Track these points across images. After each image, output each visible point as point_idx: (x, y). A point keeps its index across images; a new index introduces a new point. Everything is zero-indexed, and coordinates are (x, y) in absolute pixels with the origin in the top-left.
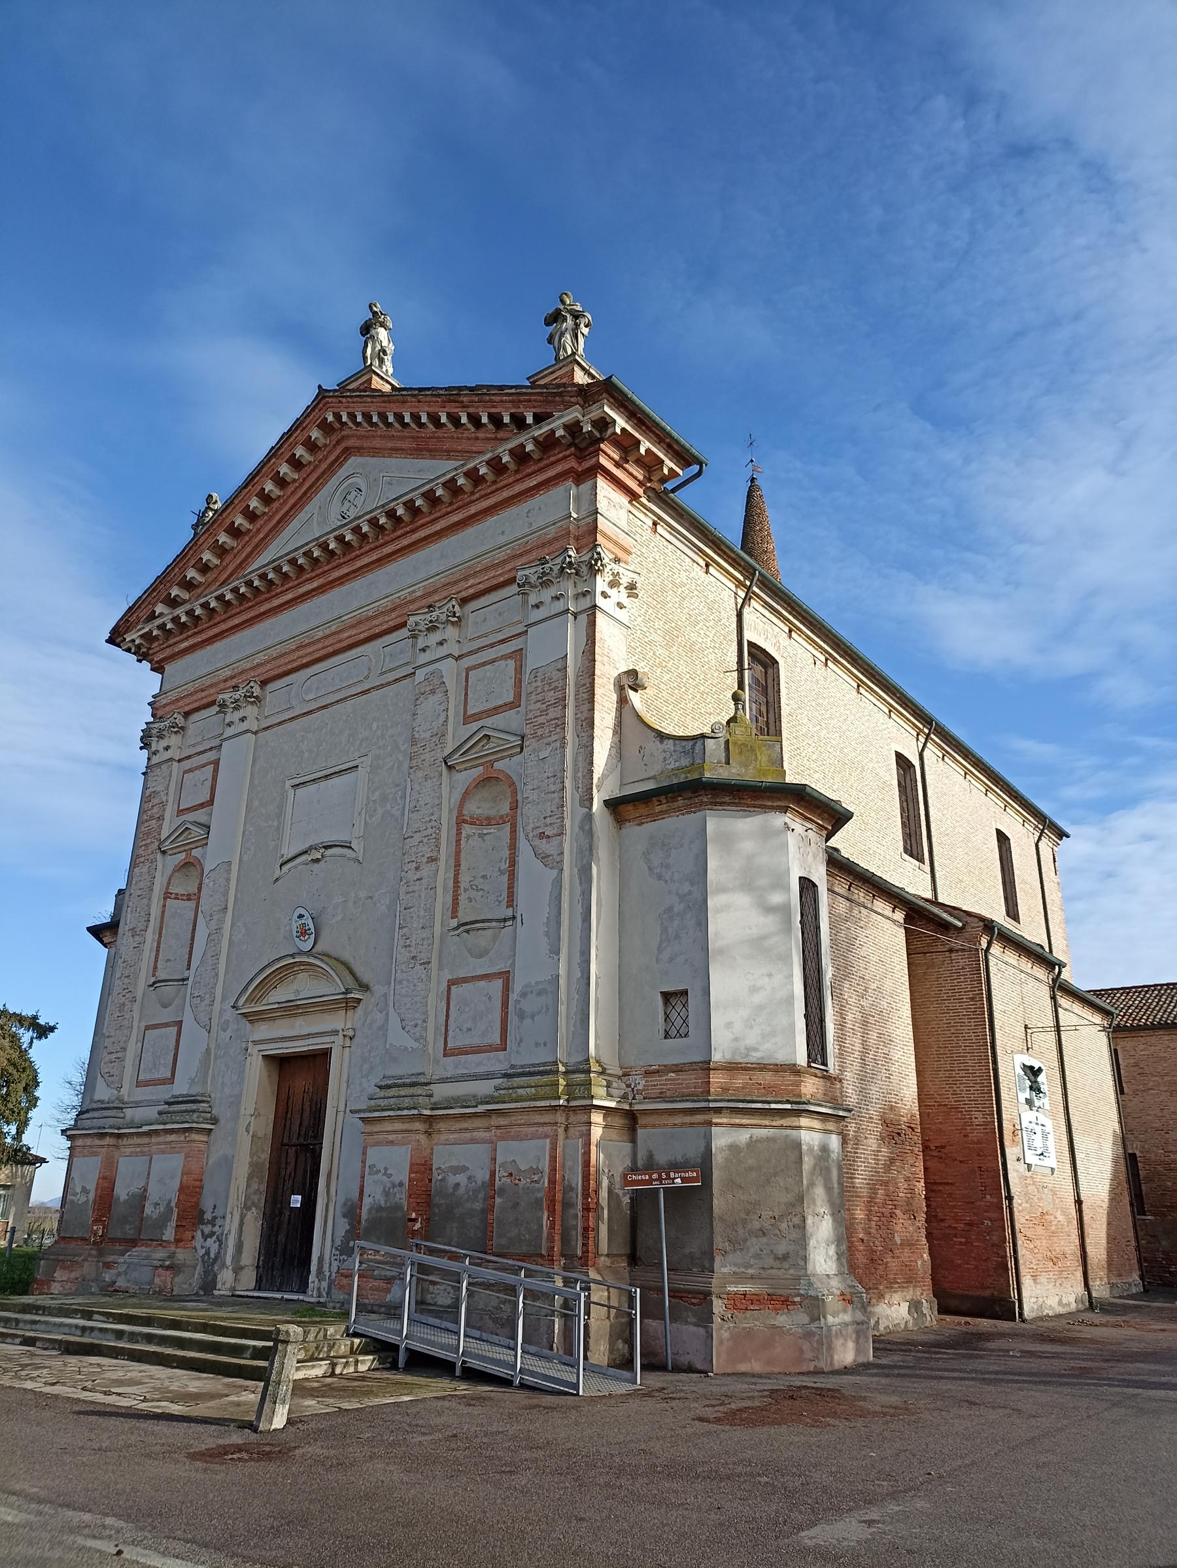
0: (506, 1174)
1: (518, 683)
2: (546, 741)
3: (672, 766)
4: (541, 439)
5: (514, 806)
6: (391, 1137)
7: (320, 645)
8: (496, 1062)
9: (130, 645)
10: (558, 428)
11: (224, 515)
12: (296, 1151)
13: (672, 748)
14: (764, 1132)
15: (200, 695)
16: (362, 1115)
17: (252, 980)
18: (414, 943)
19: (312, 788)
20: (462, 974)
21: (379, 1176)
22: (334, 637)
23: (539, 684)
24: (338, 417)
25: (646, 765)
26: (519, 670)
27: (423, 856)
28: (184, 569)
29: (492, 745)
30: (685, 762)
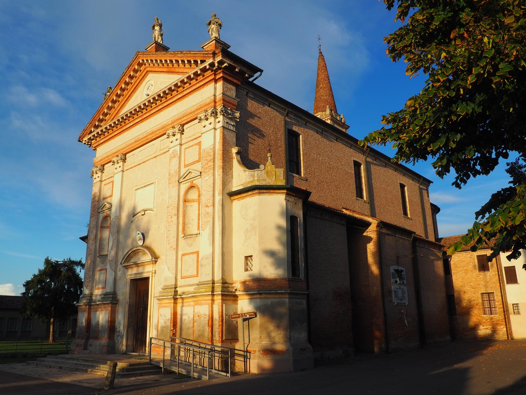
1: (200, 154)
2: (207, 174)
3: (248, 181)
6: (166, 305)
7: (142, 141)
8: (196, 281)
9: (85, 142)
11: (110, 96)
12: (143, 309)
14: (276, 300)
19: (141, 190)
22: (145, 138)
23: (205, 154)
24: (143, 60)
26: (200, 149)
28: (99, 116)
29: (192, 175)
30: (252, 179)
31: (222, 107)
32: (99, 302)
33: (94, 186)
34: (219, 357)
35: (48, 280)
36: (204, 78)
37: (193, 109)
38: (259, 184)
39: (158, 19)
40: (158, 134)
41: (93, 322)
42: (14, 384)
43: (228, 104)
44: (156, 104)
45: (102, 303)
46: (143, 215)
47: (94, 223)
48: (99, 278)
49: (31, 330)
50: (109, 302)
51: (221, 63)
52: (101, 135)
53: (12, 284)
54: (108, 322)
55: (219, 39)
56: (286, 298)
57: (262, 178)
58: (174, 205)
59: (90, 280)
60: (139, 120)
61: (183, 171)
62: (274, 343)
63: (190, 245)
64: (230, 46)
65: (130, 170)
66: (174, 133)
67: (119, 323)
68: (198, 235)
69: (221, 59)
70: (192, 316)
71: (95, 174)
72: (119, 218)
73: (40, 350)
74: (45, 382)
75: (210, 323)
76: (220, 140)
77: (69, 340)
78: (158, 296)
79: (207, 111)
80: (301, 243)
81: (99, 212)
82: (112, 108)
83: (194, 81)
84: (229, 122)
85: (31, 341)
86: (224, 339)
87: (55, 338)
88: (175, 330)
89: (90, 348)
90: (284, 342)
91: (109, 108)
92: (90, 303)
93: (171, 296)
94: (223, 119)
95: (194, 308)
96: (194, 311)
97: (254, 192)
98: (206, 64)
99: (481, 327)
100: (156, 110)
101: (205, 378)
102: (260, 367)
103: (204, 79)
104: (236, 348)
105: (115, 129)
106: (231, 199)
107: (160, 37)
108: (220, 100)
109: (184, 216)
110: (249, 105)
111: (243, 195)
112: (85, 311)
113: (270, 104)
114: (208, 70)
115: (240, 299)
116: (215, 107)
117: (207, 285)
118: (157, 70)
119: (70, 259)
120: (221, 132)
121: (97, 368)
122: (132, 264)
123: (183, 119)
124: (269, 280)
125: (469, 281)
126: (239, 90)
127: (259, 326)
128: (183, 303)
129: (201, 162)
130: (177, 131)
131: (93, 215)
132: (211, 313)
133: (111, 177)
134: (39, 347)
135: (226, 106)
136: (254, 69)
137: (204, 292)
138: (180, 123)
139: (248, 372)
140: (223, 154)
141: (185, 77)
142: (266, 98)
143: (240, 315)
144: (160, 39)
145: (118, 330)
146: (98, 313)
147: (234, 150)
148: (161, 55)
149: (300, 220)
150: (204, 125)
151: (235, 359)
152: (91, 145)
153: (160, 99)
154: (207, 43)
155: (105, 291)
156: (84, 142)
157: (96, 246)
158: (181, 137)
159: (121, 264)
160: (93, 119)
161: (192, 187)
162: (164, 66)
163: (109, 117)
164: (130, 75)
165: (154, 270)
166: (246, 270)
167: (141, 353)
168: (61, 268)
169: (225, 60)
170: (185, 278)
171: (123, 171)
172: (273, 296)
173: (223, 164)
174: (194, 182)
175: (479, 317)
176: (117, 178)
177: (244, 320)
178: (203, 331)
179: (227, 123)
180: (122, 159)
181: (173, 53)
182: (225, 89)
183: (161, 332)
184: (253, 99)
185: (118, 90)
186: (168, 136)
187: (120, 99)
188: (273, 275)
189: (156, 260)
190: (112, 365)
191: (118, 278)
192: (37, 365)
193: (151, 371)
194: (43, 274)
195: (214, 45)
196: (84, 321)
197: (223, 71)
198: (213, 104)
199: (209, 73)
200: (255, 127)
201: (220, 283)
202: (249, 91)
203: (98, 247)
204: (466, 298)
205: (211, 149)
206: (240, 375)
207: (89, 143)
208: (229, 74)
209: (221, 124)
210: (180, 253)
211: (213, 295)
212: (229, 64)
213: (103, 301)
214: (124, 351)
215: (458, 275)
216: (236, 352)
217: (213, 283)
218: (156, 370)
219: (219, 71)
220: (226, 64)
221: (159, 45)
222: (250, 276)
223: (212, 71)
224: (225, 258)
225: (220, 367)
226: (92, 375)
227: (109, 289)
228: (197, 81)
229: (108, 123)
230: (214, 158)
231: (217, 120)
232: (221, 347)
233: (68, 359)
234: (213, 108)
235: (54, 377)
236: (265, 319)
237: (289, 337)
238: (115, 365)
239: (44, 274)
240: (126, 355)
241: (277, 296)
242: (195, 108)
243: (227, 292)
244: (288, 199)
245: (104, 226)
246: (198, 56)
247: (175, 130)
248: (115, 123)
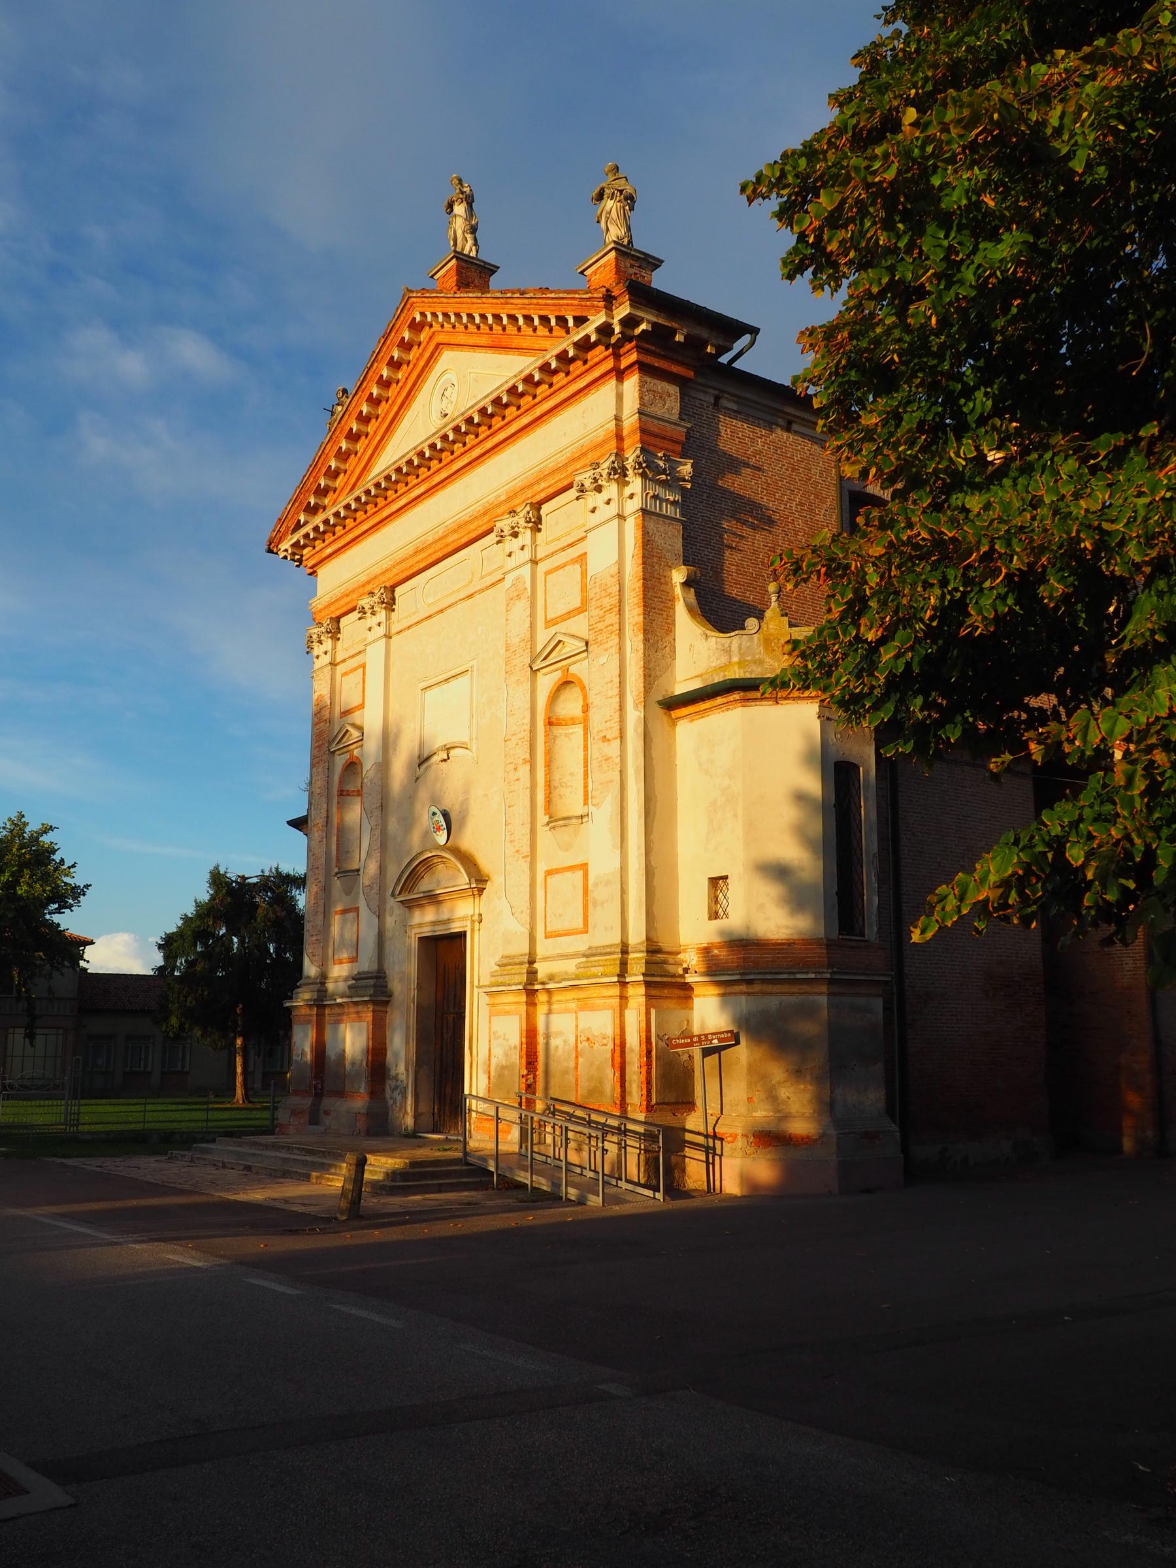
1: (584, 588)
2: (605, 646)
3: (713, 665)
4: (581, 343)
5: (586, 708)
6: (507, 1008)
8: (580, 944)
9: (285, 553)
11: (343, 422)
14: (793, 999)
16: (488, 990)
17: (403, 872)
19: (437, 689)
23: (598, 590)
24: (423, 314)
26: (584, 574)
28: (316, 478)
29: (567, 649)
30: (724, 660)
31: (638, 452)
32: (342, 997)
33: (316, 678)
34: (640, 1149)
35: (223, 931)
36: (587, 366)
37: (562, 459)
38: (743, 676)
39: (460, 181)
41: (331, 1053)
42: (134, 1203)
43: (657, 442)
44: (464, 444)
45: (349, 1000)
46: (445, 760)
47: (319, 783)
48: (342, 936)
49: (186, 1069)
50: (366, 999)
51: (629, 322)
52: (324, 532)
53: (132, 936)
54: (368, 1052)
55: (630, 242)
57: (753, 655)
58: (522, 735)
59: (319, 937)
61: (543, 636)
62: (786, 1117)
63: (566, 847)
64: (663, 261)
66: (516, 529)
67: (396, 1055)
68: (584, 820)
69: (628, 311)
70: (572, 1040)
71: (315, 645)
72: (384, 766)
73: (204, 1124)
74: (204, 1199)
75: (618, 1060)
76: (635, 548)
77: (277, 1099)
78: (488, 983)
79: (598, 466)
80: (869, 841)
81: (334, 752)
82: (350, 455)
83: (560, 379)
84: (662, 495)
85: (189, 1100)
86: (654, 1101)
87: (250, 1093)
88: (531, 1076)
89: (327, 1120)
91: (343, 456)
92: (321, 1001)
93: (520, 984)
94: (644, 489)
95: (577, 1018)
96: (577, 1026)
98: (590, 329)
101: (595, 1201)
102: (746, 1179)
103: (587, 371)
104: (688, 1127)
105: (360, 515)
106: (670, 716)
107: (469, 236)
108: (633, 432)
109: (548, 764)
110: (726, 432)
111: (703, 706)
112: (309, 1022)
113: (790, 423)
114: (595, 344)
115: (698, 996)
116: (619, 454)
117: (608, 957)
119: (277, 869)
120: (637, 525)
121: (333, 1171)
122: (422, 895)
123: (537, 488)
124: (773, 944)
126: (693, 393)
128: (549, 1003)
129: (586, 613)
130: (522, 522)
131: (317, 760)
132: (618, 1031)
133: (360, 652)
134: (202, 1115)
135: (652, 449)
136: (732, 329)
137: (600, 977)
138: (528, 499)
139: (718, 1191)
140: (646, 588)
141: (535, 369)
142: (775, 405)
143: (695, 1039)
144: (470, 242)
145: (393, 1073)
146: (342, 1026)
147: (678, 576)
148: (467, 300)
149: (867, 773)
150: (591, 507)
151: (685, 1156)
152: (300, 561)
153: (472, 429)
154: (594, 260)
155: (356, 969)
156: (282, 555)
157: (328, 845)
158: (534, 540)
159: (393, 895)
160: (302, 490)
161: (566, 683)
162: (482, 331)
163: (345, 480)
164: (392, 357)
165: (477, 912)
166: (714, 915)
167: (454, 1134)
168: (255, 898)
169: (640, 314)
170: (556, 936)
171: (388, 636)
172: (785, 988)
173: (644, 618)
174: (572, 669)
176: (375, 656)
177: (707, 1053)
178: (601, 1081)
179: (655, 497)
180: (383, 602)
181: (499, 295)
182: (646, 398)
183: (498, 1081)
184: (735, 414)
185: (361, 405)
186: (498, 538)
187: (370, 429)
188: (785, 931)
189: (480, 886)
190: (354, 1162)
191: (388, 934)
192: (192, 1161)
193: (465, 1180)
194: (205, 912)
195: (613, 265)
196: (308, 1049)
197: (637, 346)
198: (613, 444)
199: (599, 352)
200: (742, 497)
201: (642, 952)
202: (722, 391)
203: (334, 847)
205: (612, 576)
206: (693, 1197)
207: (297, 557)
208: (658, 351)
209: (633, 506)
210: (541, 868)
211: (623, 984)
212: (654, 325)
213: (351, 997)
214: (409, 1128)
216: (689, 1137)
217: (625, 951)
218: (478, 1180)
219: (628, 346)
220: (643, 326)
221: (466, 261)
222: (722, 933)
223: (607, 349)
224: (657, 881)
225: (641, 1175)
226: (320, 1187)
227: (366, 964)
228: (570, 378)
229: (341, 498)
230: (621, 602)
231: (628, 491)
232: (645, 1123)
233: (266, 1147)
234: (613, 458)
235: (228, 1190)
236: (759, 1052)
237: (828, 1099)
238: (361, 1164)
239: (208, 915)
240: (413, 1140)
241: (795, 989)
242: (568, 454)
243: (661, 976)
244: (827, 714)
245: (348, 791)
247: (516, 518)
248: (358, 499)
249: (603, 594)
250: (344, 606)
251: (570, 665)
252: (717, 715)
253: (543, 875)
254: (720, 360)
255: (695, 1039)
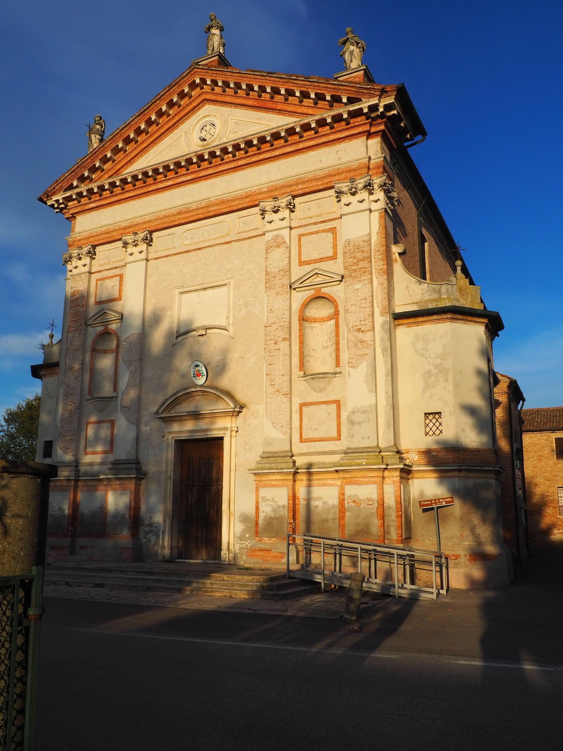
0: (352, 501)
2: (358, 279)
3: (427, 298)
6: (274, 483)
7: (194, 213)
8: (342, 445)
10: (365, 108)
11: (123, 131)
13: (427, 288)
14: (479, 481)
15: (106, 236)
18: (277, 383)
19: (194, 294)
20: (309, 400)
21: (269, 502)
23: (351, 248)
25: (410, 296)
27: (279, 337)
28: (93, 161)
30: (435, 296)
40: (233, 205)
51: (388, 107)
54: (130, 509)
56: (492, 478)
58: (282, 324)
60: (189, 177)
65: (164, 259)
69: (393, 101)
78: (254, 468)
90: (492, 543)
97: (445, 317)
98: (365, 105)
99: (556, 531)
100: (232, 166)
103: (347, 129)
108: (378, 167)
111: (421, 319)
113: (409, 188)
117: (366, 454)
118: (228, 101)
122: (186, 414)
125: (543, 471)
127: (459, 518)
143: (433, 502)
148: (254, 76)
155: (111, 458)
156: (49, 203)
160: (81, 166)
163: (112, 166)
170: (311, 441)
172: (475, 475)
175: (553, 518)
185: (141, 123)
199: (361, 120)
204: (537, 493)
215: (528, 462)
219: (380, 121)
220: (395, 112)
223: (367, 119)
246: (346, 90)
249: (356, 250)
250: (103, 239)
251: (322, 288)
252: (430, 325)
253: (298, 406)
254: (404, 144)
255: (433, 502)
